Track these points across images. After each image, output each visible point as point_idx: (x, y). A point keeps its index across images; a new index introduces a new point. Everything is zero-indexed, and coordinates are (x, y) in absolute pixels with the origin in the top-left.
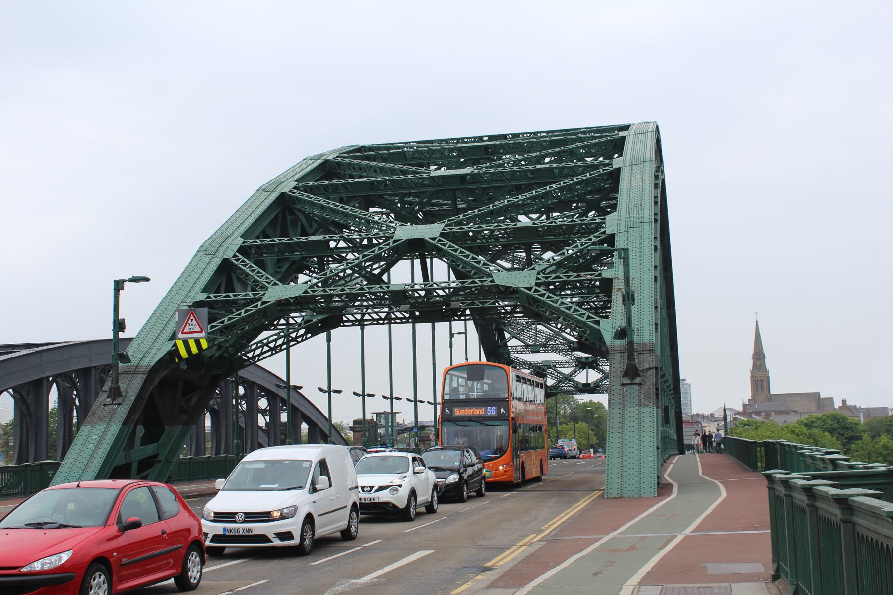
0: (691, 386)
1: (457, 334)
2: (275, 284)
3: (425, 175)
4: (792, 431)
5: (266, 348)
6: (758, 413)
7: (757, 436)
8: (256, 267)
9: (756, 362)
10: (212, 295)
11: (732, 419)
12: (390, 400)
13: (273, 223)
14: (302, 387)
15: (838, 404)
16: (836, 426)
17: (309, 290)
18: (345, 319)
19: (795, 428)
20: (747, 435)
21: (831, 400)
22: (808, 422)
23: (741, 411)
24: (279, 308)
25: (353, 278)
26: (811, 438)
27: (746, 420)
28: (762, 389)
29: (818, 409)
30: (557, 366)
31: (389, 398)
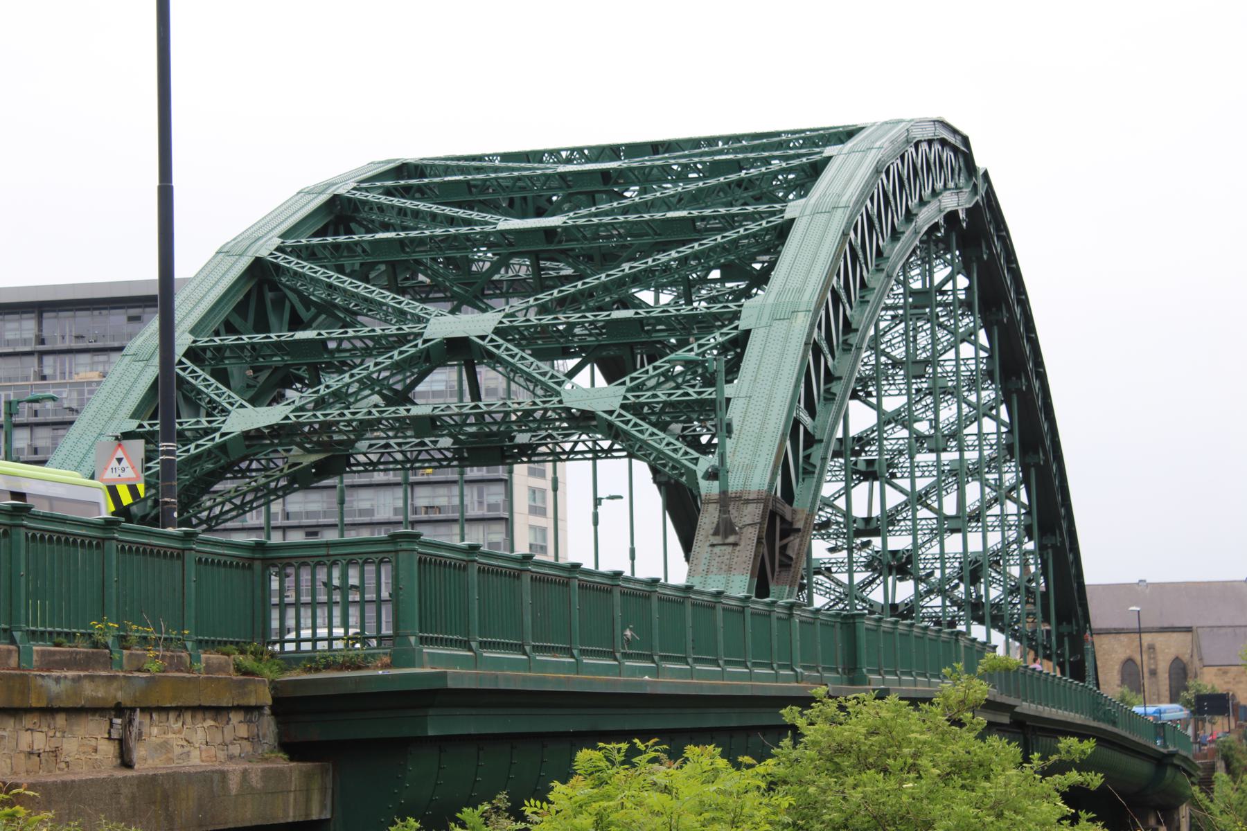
1: (608, 498)
2: (242, 406)
3: (488, 228)
5: (228, 507)
8: (212, 380)
10: (145, 423)
13: (241, 309)
17: (291, 416)
18: (352, 461)
24: (247, 443)
25: (359, 397)
30: (834, 570)
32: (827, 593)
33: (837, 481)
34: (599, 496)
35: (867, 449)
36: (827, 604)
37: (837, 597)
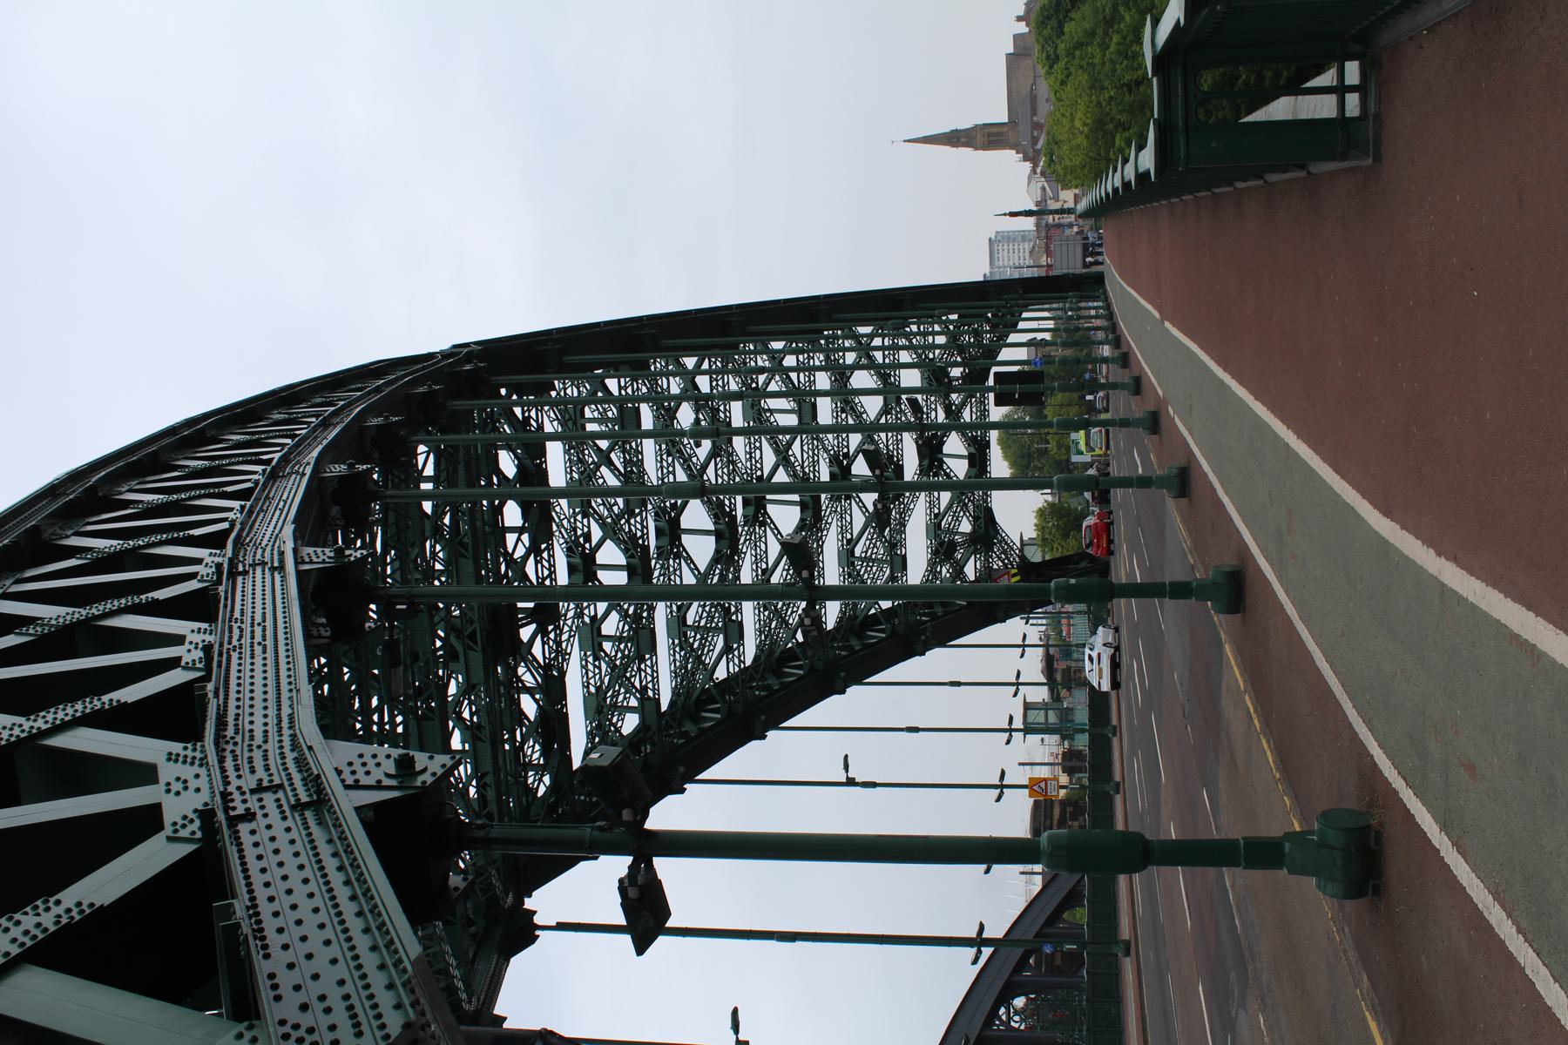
0: (999, 230)
1: (847, 771)
4: (1062, 84)
6: (1035, 141)
7: (1070, 141)
9: (963, 143)
11: (1043, 179)
14: (981, 923)
15: (1022, 28)
16: (1054, 22)
19: (1057, 79)
20: (1068, 158)
21: (1017, 38)
22: (1048, 64)
26: (1073, 54)
27: (1043, 159)
28: (1001, 134)
29: (1030, 56)
31: (1024, 650)
32: (957, 519)
33: (851, 509)
35: (728, 510)
36: (968, 518)
37: (962, 509)
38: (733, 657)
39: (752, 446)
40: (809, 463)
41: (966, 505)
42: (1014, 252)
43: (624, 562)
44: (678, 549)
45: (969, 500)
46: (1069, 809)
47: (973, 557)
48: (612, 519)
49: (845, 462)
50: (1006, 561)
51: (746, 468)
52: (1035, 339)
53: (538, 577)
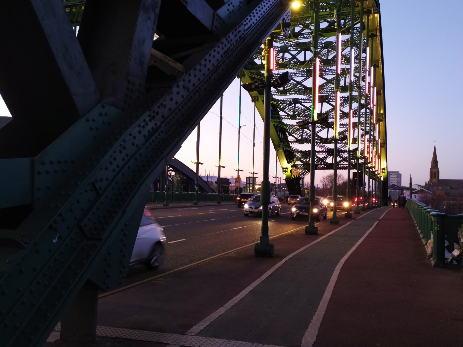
0: (402, 175)
12: (275, 178)
23: (424, 186)
28: (435, 177)
34: (240, 125)
35: (321, 91)
37: (317, 161)
38: (276, 92)
39: (344, 125)
40: (327, 90)
41: (318, 162)
42: (394, 176)
43: (323, 112)
44: (324, 128)
45: (319, 163)
46: (227, 189)
47: (302, 164)
48: (320, 56)
49: (327, 100)
50: (300, 173)
51: (333, 96)
52: (366, 185)
53: (304, 33)
